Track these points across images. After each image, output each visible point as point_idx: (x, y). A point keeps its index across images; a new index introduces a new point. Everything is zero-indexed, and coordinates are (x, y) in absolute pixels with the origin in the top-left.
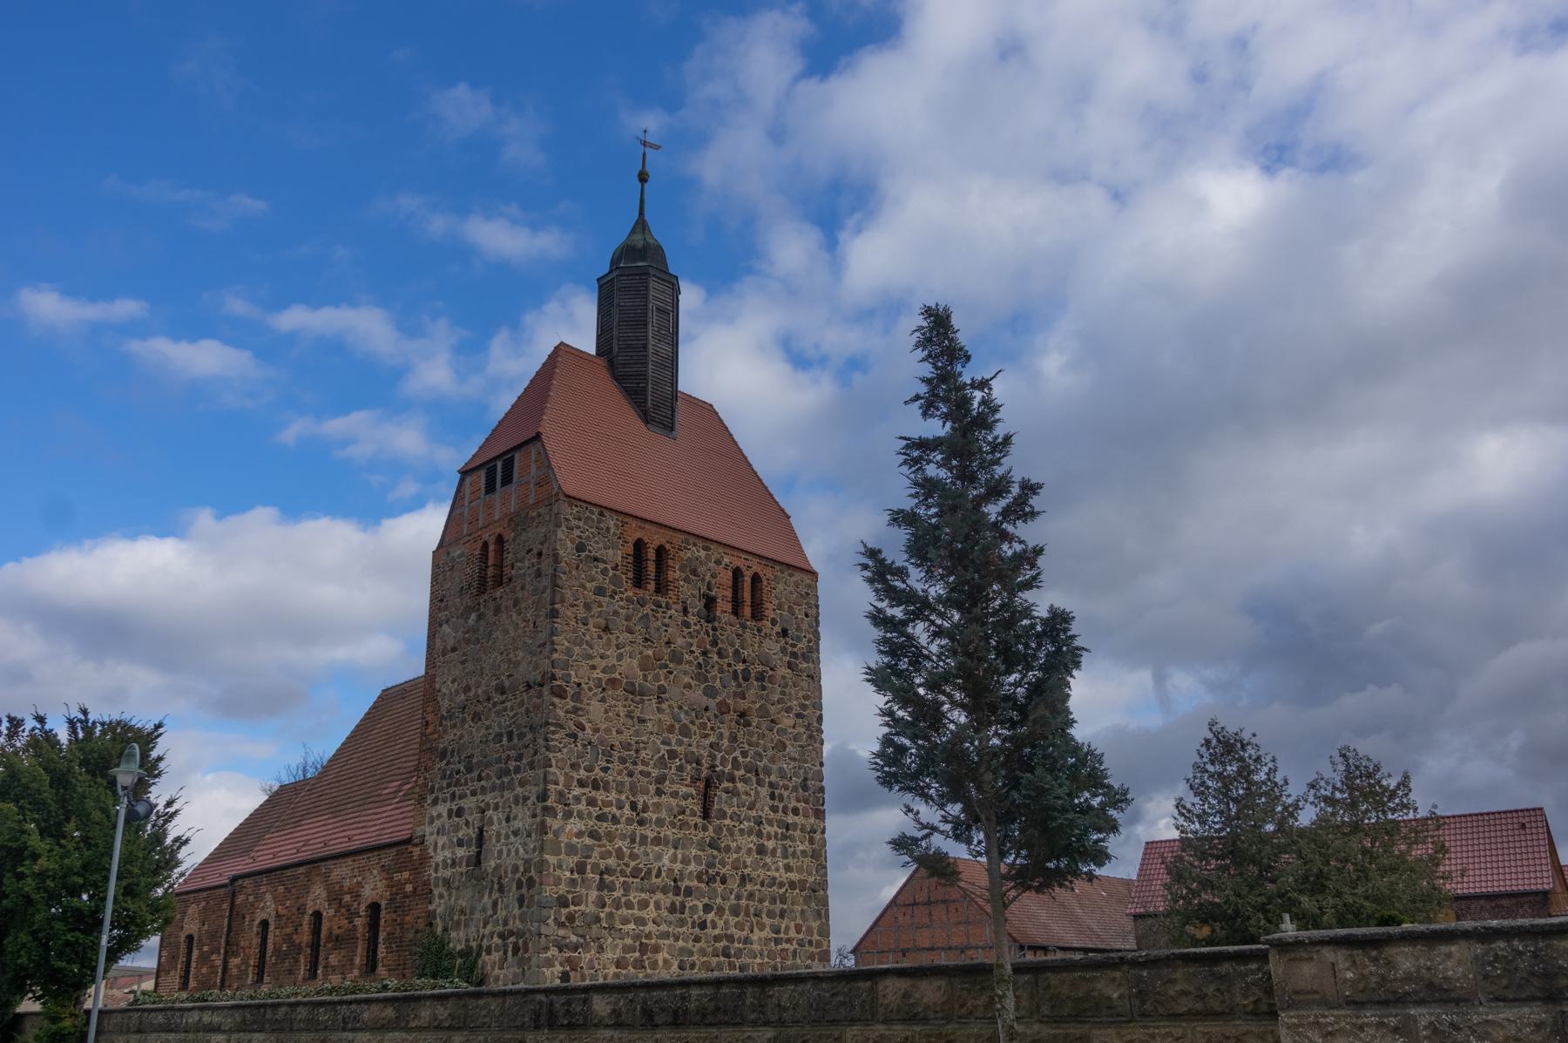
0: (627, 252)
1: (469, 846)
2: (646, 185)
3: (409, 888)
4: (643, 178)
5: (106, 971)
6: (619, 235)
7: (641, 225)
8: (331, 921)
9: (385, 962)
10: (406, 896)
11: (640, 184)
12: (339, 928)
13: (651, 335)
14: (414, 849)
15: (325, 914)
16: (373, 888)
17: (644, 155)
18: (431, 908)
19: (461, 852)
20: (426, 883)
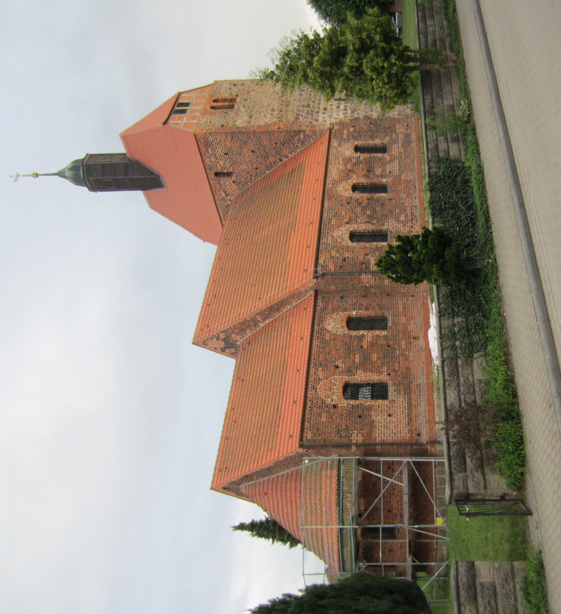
0: (77, 180)
1: (340, 103)
2: (39, 173)
3: (351, 129)
4: (37, 175)
5: (431, 491)
6: (67, 184)
7: (61, 174)
8: (359, 176)
9: (383, 138)
10: (354, 131)
11: (40, 177)
12: (363, 170)
13: (280, 474)
14: (335, 129)
15: (354, 181)
16: (348, 151)
17: (23, 176)
18: (362, 117)
19: (342, 107)
20: (351, 121)
